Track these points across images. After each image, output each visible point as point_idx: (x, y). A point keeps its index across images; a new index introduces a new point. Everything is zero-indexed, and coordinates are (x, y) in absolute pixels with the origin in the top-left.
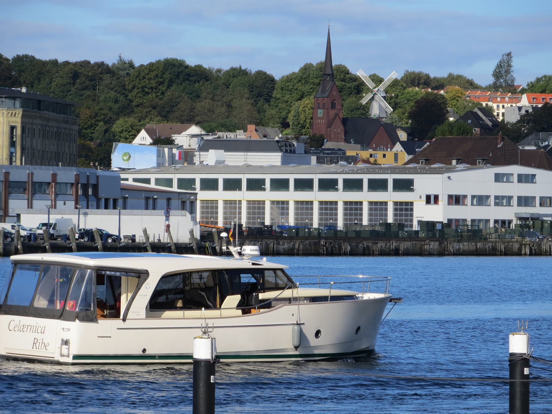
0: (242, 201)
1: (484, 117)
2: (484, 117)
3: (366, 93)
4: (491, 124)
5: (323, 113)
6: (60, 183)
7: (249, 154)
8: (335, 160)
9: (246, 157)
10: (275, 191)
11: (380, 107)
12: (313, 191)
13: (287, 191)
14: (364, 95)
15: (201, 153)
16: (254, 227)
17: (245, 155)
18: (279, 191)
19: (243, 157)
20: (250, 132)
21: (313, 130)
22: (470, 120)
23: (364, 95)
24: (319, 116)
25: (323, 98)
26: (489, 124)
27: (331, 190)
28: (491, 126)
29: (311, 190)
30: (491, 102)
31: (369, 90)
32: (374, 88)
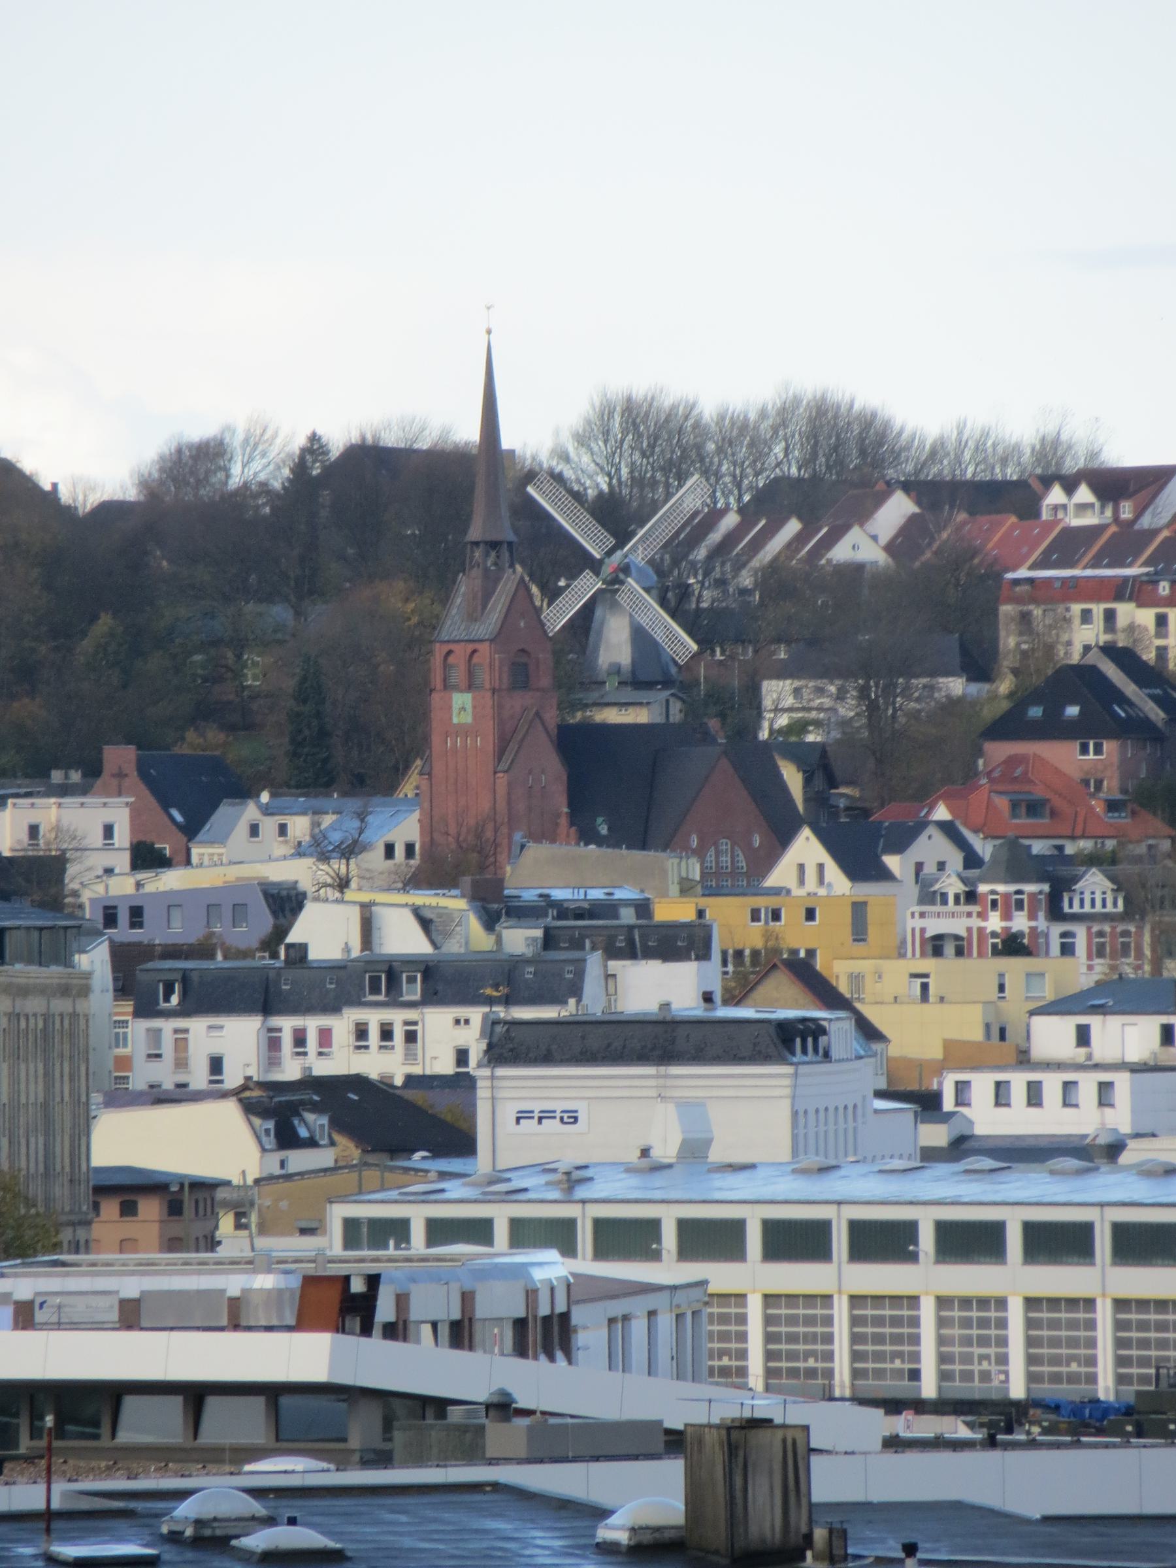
0: (836, 1297)
1: (1130, 689)
2: (1130, 689)
3: (573, 576)
4: (1162, 715)
5: (474, 707)
6: (485, 1320)
7: (675, 1070)
8: (621, 941)
9: (661, 1082)
10: (956, 1263)
11: (640, 637)
12: (1093, 1264)
13: (996, 1263)
14: (562, 583)
15: (501, 1071)
16: (401, 1249)
17: (657, 1077)
18: (971, 1263)
19: (653, 1082)
20: (113, 775)
21: (430, 779)
22: (1073, 702)
23: (562, 583)
24: (455, 720)
25: (471, 647)
26: (1152, 716)
27: (1160, 1262)
28: (1160, 724)
29: (1088, 1261)
30: (1130, 599)
31: (584, 562)
32: (610, 553)
